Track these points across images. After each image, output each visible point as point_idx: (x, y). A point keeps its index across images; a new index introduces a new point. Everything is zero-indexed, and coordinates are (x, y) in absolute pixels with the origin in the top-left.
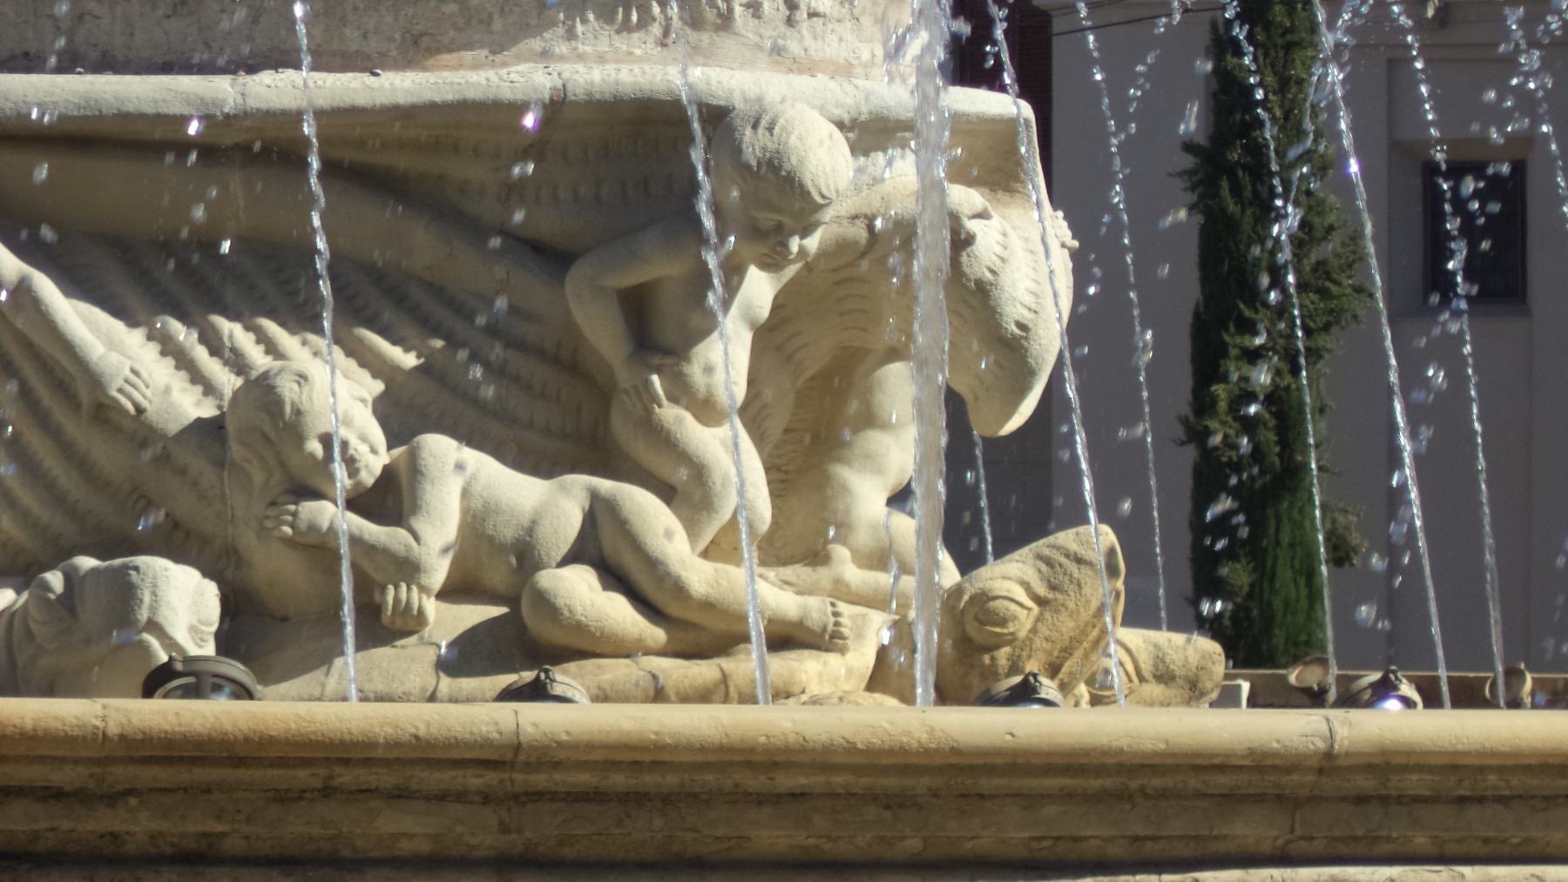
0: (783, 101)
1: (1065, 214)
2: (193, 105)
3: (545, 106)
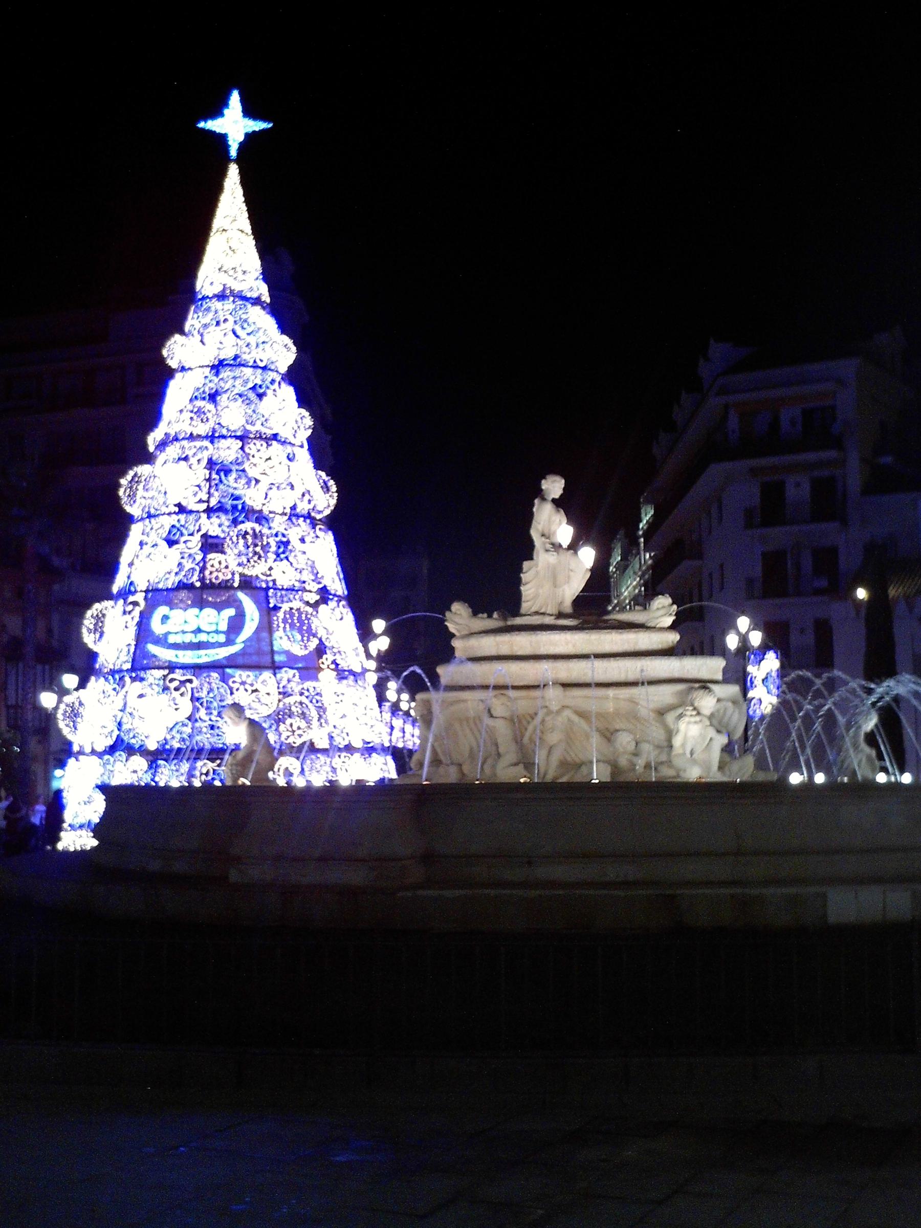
0: (327, 777)
1: (57, 842)
2: (340, 750)
3: (317, 470)
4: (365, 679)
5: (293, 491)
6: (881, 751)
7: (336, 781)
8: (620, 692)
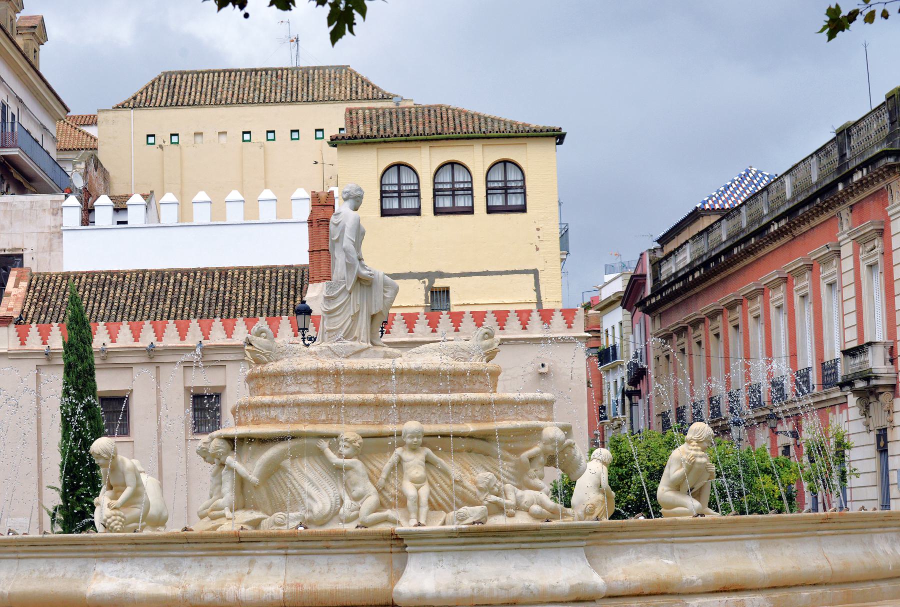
4: (489, 435)
5: (245, 19)
6: (256, 550)
7: (682, 336)
8: (709, 600)
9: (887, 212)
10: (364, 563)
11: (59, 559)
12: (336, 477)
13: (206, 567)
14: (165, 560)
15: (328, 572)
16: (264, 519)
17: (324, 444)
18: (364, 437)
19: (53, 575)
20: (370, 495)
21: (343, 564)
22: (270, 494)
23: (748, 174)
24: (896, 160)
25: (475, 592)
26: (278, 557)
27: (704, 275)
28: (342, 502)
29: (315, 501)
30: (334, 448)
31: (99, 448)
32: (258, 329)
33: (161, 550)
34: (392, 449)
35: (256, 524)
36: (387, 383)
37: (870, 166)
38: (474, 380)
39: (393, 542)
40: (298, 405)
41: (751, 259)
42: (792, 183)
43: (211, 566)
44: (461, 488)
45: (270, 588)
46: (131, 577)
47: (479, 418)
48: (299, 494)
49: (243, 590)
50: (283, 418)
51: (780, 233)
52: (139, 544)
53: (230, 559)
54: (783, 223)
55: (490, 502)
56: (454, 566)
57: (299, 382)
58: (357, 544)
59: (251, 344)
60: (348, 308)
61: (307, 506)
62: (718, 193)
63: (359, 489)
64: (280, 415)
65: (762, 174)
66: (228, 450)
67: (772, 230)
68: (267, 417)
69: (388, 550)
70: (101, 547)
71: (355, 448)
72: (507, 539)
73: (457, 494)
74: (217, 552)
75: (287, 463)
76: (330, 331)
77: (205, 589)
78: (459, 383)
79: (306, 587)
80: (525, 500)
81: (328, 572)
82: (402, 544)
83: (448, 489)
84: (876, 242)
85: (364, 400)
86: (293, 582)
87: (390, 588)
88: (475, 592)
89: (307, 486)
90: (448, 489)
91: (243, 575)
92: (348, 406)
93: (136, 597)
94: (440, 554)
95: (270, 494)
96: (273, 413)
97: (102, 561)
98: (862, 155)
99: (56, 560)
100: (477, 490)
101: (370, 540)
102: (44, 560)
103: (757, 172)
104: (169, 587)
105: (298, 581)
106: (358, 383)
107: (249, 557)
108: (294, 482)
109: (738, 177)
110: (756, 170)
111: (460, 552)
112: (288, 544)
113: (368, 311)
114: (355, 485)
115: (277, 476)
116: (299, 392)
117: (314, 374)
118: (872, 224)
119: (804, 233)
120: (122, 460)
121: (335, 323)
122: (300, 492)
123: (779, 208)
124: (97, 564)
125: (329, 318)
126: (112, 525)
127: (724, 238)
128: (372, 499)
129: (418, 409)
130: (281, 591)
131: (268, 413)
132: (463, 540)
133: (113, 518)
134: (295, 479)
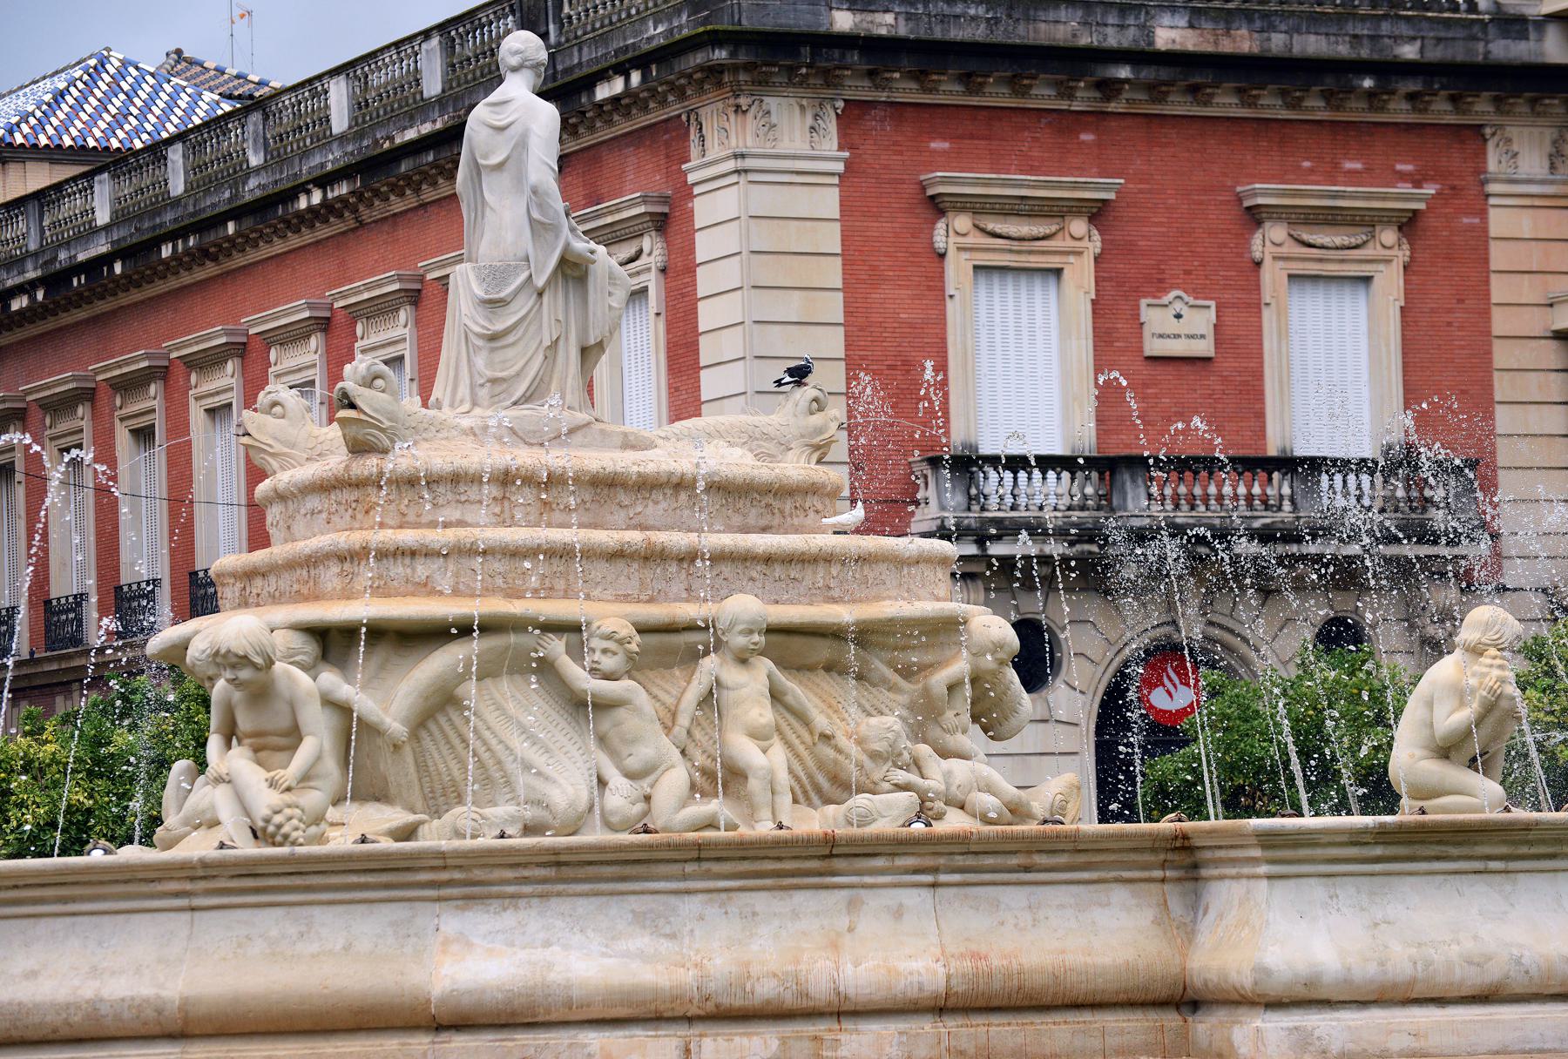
9: (685, 174)
10: (1109, 904)
11: (325, 908)
12: (578, 722)
13: (742, 916)
14: (634, 903)
15: (1034, 926)
16: (422, 823)
17: (556, 646)
18: (643, 629)
19: (314, 948)
20: (673, 766)
21: (1061, 906)
22: (422, 767)
23: (103, 66)
24: (733, 54)
25: (1419, 969)
26: (915, 891)
27: (42, 305)
28: (602, 783)
29: (547, 779)
30: (577, 653)
31: (244, 642)
32: (368, 368)
33: (623, 879)
34: (693, 656)
35: (408, 833)
36: (646, 506)
37: (654, 67)
38: (807, 505)
39: (1170, 856)
40: (470, 551)
41: (211, 269)
42: (352, 96)
43: (754, 914)
44: (831, 753)
45: (914, 964)
46: (547, 944)
47: (836, 593)
48: (499, 762)
49: (849, 969)
50: (445, 585)
51: (328, 210)
52: (566, 864)
53: (799, 897)
54: (343, 189)
55: (895, 785)
56: (1363, 909)
57: (463, 498)
58: (1094, 860)
59: (352, 406)
60: (533, 328)
61: (521, 792)
62: (39, 108)
63: (639, 755)
64: (437, 577)
65: (137, 68)
66: (316, 658)
67: (303, 203)
68: (407, 581)
69: (1158, 874)
70: (457, 875)
71: (630, 657)
72: (1465, 851)
73: (821, 765)
74: (768, 882)
75: (470, 689)
76: (494, 381)
77: (755, 970)
78: (782, 512)
79: (996, 962)
80: (958, 782)
81: (1034, 926)
82: (1188, 861)
83: (805, 754)
84: (646, 243)
85: (623, 545)
86: (962, 950)
87: (1177, 961)
88: (1419, 969)
89: (521, 746)
90: (805, 754)
91: (839, 935)
92: (588, 558)
93: (575, 993)
94: (1330, 881)
95: (422, 767)
96: (422, 569)
97: (457, 907)
98: (603, 39)
99: (316, 911)
100: (864, 758)
101: (1121, 851)
102: (279, 911)
103: (125, 63)
104: (660, 967)
105: (974, 947)
106: (588, 505)
107: (844, 893)
108: (487, 734)
109: (81, 72)
110: (121, 57)
111: (1368, 878)
112: (942, 861)
113: (584, 330)
114: (634, 741)
115: (442, 720)
116: (461, 523)
117: (498, 480)
118: (645, 200)
119: (395, 214)
120: (289, 676)
121: (504, 362)
122: (503, 758)
123: (305, 154)
124: (443, 918)
125: (493, 350)
126: (286, 829)
127: (103, 217)
128: (676, 778)
129: (724, 568)
130: (941, 971)
131: (409, 571)
132: (1378, 851)
133: (288, 811)
134: (489, 728)
